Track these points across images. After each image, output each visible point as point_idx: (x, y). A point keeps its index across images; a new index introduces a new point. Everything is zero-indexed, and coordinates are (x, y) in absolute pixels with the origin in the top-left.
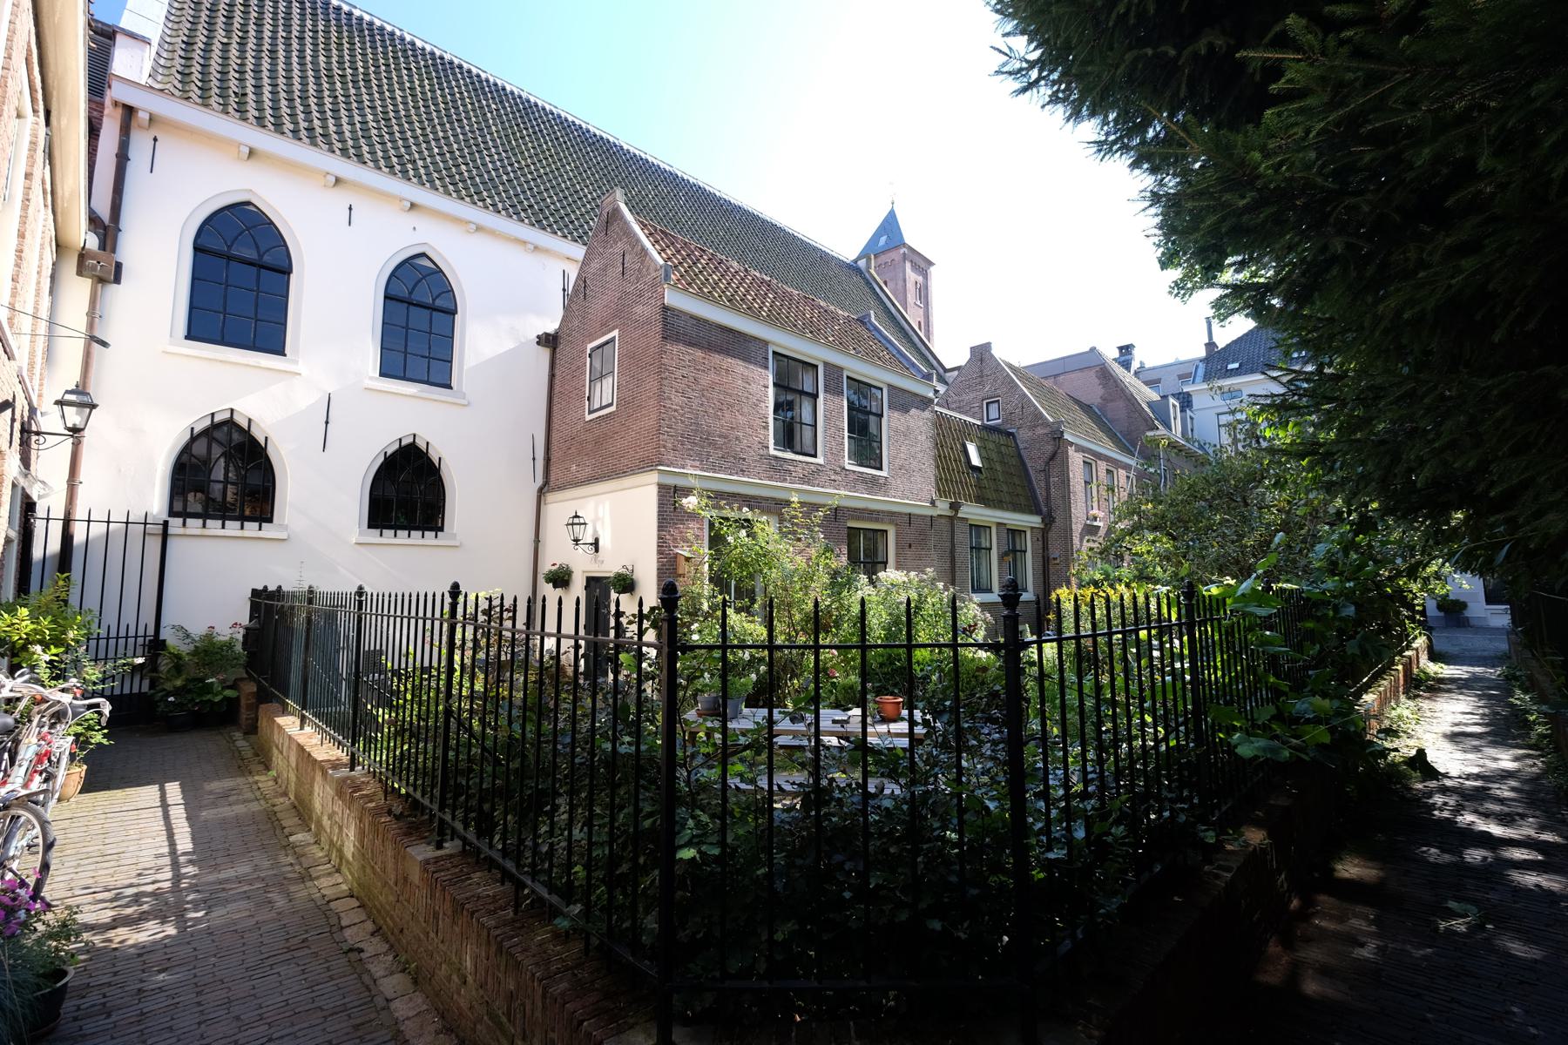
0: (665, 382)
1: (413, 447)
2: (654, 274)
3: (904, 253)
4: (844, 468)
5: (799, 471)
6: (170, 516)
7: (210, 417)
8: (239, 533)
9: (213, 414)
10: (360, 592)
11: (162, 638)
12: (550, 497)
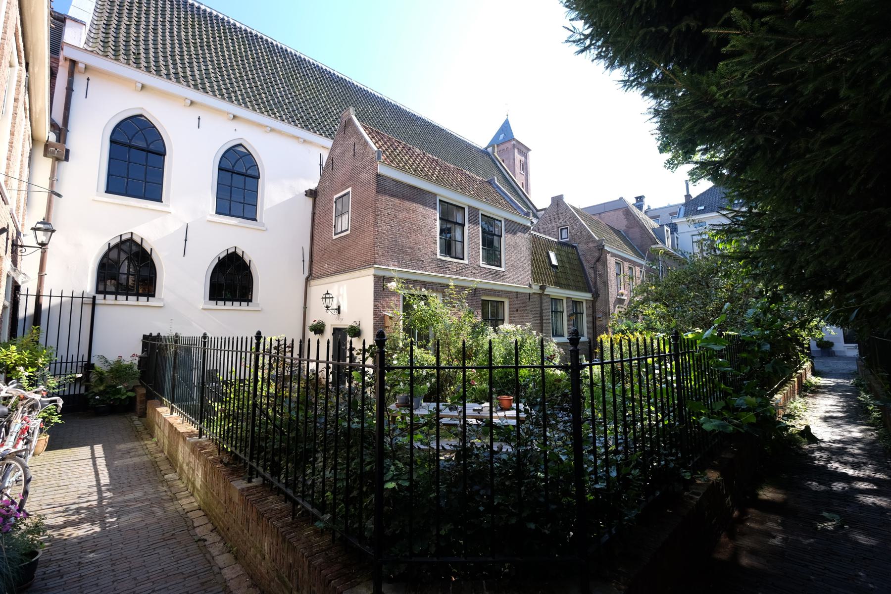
0: (378, 217)
1: (235, 254)
2: (372, 156)
3: (514, 144)
4: (479, 266)
5: (454, 268)
6: (96, 293)
7: (119, 237)
8: (136, 303)
9: (121, 236)
10: (205, 337)
11: (92, 362)
12: (313, 283)
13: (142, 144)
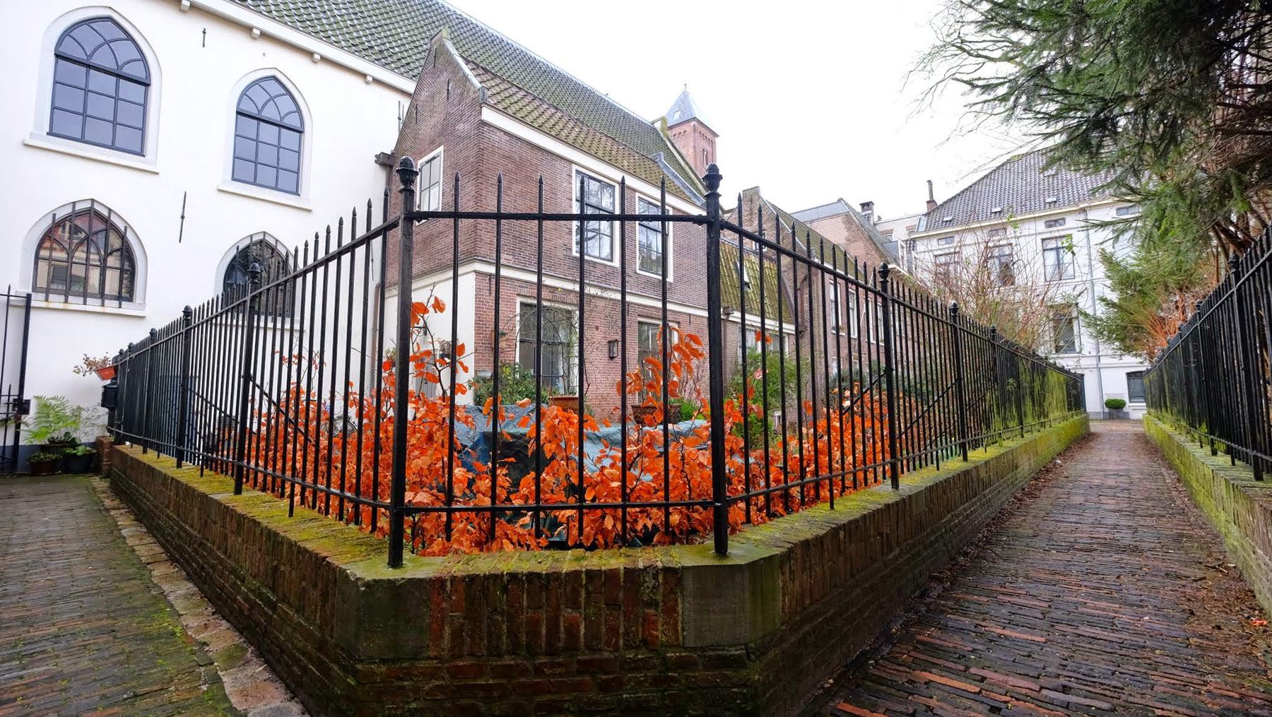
0: (483, 187)
2: (472, 96)
3: (694, 126)
4: (636, 273)
6: (33, 291)
7: (71, 206)
8: (100, 309)
9: (74, 203)
11: (25, 398)
13: (110, 65)
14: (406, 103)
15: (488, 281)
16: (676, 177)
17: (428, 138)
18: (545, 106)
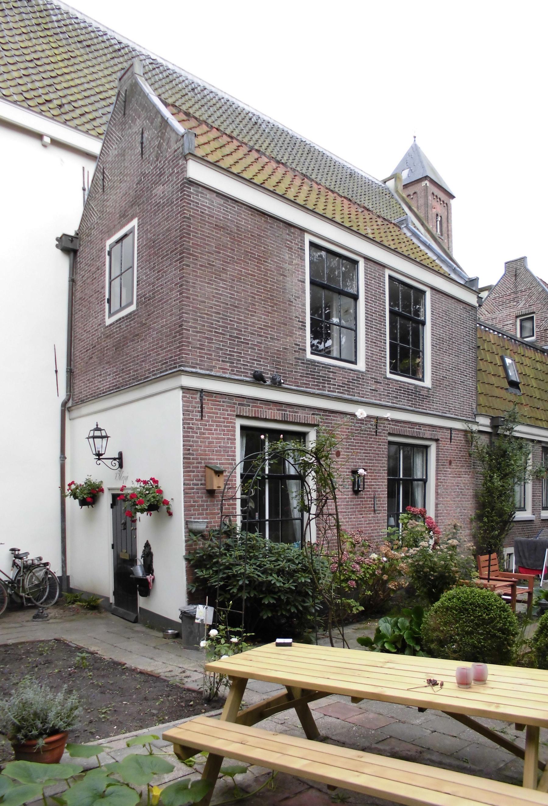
4: (386, 378)
5: (339, 379)
14: (91, 167)
15: (198, 400)
16: (429, 247)
17: (118, 211)
18: (265, 159)
